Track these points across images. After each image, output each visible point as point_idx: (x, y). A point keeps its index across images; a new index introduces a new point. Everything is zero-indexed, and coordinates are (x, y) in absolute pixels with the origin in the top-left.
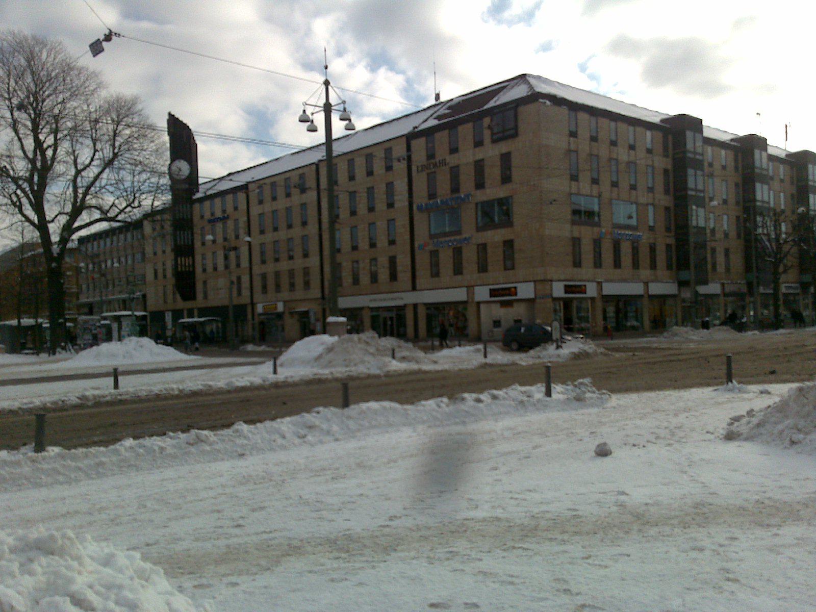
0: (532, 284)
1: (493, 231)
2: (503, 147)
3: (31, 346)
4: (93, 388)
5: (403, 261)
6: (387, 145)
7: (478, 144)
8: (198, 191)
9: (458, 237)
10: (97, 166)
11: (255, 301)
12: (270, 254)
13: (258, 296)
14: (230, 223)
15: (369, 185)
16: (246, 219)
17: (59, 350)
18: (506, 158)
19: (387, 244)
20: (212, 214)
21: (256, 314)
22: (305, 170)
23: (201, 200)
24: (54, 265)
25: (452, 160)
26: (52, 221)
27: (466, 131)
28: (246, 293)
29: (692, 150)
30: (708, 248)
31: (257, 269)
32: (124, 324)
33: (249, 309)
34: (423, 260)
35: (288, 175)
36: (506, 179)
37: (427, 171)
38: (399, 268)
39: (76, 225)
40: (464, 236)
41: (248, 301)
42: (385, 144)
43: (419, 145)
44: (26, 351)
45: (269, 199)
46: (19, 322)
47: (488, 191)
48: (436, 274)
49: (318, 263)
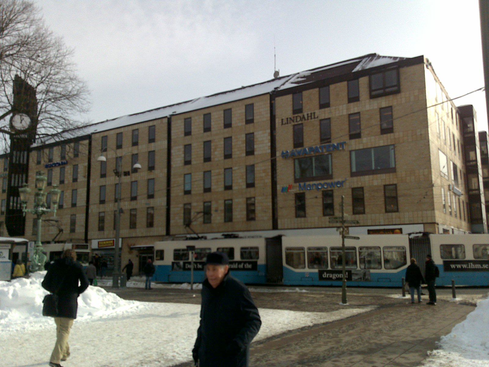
0: (422, 225)
1: (371, 176)
2: (383, 102)
5: (263, 204)
6: (188, 116)
7: (353, 98)
8: (35, 142)
9: (329, 181)
13: (93, 232)
14: (69, 169)
15: (227, 135)
16: (86, 164)
19: (244, 186)
20: (50, 160)
22: (155, 123)
23: (38, 149)
25: (323, 114)
27: (339, 90)
29: (194, 180)
31: (94, 209)
34: (287, 203)
35: (135, 127)
36: (387, 130)
37: (293, 124)
38: (258, 208)
40: (336, 180)
42: (246, 100)
43: (285, 107)
47: (364, 140)
49: (164, 203)
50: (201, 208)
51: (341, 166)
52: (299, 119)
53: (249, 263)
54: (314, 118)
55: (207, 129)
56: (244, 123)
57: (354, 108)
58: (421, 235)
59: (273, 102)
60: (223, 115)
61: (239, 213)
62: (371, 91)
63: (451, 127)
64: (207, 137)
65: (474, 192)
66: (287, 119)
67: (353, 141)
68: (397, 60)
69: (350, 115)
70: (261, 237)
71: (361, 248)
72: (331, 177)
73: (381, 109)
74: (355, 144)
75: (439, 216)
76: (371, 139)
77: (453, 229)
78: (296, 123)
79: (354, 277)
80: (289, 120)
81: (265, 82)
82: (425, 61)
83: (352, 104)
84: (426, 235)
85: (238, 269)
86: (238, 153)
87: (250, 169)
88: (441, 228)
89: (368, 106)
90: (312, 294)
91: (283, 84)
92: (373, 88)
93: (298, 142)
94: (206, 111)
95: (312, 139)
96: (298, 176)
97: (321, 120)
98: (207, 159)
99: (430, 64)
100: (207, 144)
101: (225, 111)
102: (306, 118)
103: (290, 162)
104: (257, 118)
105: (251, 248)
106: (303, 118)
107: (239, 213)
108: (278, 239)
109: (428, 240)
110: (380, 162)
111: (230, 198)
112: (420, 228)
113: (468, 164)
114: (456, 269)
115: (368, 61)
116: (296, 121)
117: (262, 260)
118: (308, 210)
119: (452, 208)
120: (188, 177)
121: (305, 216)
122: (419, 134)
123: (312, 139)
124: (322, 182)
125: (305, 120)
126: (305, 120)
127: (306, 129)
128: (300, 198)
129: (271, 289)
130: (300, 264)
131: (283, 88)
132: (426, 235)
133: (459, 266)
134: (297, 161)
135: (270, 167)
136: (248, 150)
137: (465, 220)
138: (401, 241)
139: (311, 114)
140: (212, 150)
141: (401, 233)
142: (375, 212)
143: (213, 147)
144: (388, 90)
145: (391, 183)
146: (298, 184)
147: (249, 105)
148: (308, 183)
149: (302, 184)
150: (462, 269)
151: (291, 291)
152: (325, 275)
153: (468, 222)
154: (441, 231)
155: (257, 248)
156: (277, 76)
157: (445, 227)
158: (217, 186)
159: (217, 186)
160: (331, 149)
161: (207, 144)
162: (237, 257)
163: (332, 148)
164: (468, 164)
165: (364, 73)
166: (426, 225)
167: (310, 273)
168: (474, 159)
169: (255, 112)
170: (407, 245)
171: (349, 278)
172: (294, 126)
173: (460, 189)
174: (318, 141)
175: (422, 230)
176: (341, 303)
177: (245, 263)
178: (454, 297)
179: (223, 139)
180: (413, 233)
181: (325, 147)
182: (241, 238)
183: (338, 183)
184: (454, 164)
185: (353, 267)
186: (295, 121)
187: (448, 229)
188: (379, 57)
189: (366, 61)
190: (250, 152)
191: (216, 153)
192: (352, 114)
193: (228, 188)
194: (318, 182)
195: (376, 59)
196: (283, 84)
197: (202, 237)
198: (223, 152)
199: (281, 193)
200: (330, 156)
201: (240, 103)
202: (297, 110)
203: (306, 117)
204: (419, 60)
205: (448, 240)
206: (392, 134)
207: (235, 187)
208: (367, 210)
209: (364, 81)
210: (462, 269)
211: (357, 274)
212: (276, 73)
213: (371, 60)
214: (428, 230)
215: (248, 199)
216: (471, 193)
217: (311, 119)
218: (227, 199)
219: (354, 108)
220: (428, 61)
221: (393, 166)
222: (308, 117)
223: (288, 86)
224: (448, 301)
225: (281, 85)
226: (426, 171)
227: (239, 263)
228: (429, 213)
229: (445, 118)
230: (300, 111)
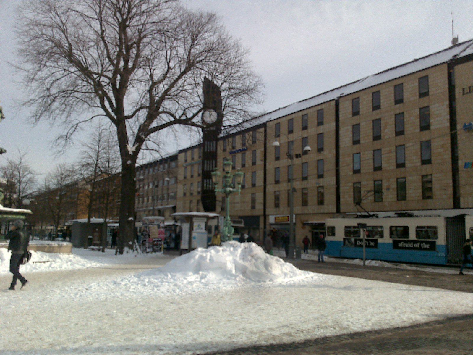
3: (98, 242)
6: (356, 96)
8: (221, 133)
10: (178, 69)
11: (267, 213)
12: (283, 176)
14: (248, 154)
16: (263, 149)
17: (126, 249)
20: (234, 147)
21: (267, 223)
22: (323, 106)
23: (224, 138)
24: (129, 162)
26: (131, 117)
28: (259, 206)
30: (109, 230)
31: (270, 189)
32: (196, 225)
33: (262, 220)
35: (304, 112)
38: (436, 186)
39: (154, 124)
41: (261, 213)
44: (92, 247)
45: (286, 132)
46: (89, 220)
49: (334, 182)
50: (371, 186)
53: (427, 243)
55: (376, 107)
56: (418, 97)
59: (451, 71)
61: (414, 191)
70: (439, 216)
85: (414, 248)
87: (426, 145)
91: (464, 50)
94: (375, 89)
100: (377, 123)
107: (414, 191)
117: (441, 240)
131: (463, 54)
140: (382, 128)
147: (423, 79)
155: (435, 228)
156: (455, 43)
158: (388, 163)
159: (388, 163)
161: (377, 123)
162: (412, 236)
177: (422, 242)
179: (394, 116)
182: (417, 216)
190: (425, 126)
191: (386, 131)
196: (464, 50)
197: (374, 215)
201: (412, 77)
207: (408, 165)
212: (455, 40)
218: (398, 177)
227: (415, 242)
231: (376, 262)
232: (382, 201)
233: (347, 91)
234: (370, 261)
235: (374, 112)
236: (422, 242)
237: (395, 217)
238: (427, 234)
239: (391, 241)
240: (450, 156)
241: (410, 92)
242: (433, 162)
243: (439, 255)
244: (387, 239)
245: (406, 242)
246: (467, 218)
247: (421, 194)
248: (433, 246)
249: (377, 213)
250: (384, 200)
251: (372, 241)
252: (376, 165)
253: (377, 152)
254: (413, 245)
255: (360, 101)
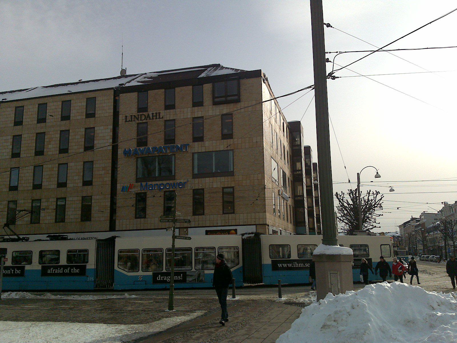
1: (211, 179)
2: (225, 109)
4: (435, 293)
5: (100, 205)
6: (20, 104)
7: (198, 103)
9: (171, 182)
18: (227, 117)
19: (81, 184)
25: (169, 115)
27: (184, 93)
34: (126, 203)
36: (227, 136)
37: (138, 122)
38: (95, 208)
40: (178, 181)
43: (129, 104)
47: (207, 143)
48: (141, 212)
50: (28, 206)
51: (183, 168)
52: (143, 118)
53: (77, 267)
54: (159, 118)
55: (42, 120)
56: (84, 117)
57: (198, 112)
58: (253, 235)
59: (117, 98)
60: (60, 107)
61: (73, 212)
62: (214, 97)
63: (282, 139)
64: (41, 128)
65: (299, 198)
66: (131, 116)
67: (196, 144)
68: (239, 71)
69: (194, 118)
70: (92, 238)
71: (197, 249)
72: (174, 178)
73: (223, 115)
74: (197, 147)
75: (270, 219)
76: (212, 144)
77: (281, 231)
78: (140, 122)
79: (189, 279)
80: (133, 117)
81: (111, 79)
82: (262, 75)
83: (196, 108)
84: (257, 235)
85: (64, 274)
86: (76, 147)
87: (88, 165)
88: (271, 229)
89: (211, 112)
90: (141, 299)
91: (129, 82)
92: (216, 96)
93: (142, 142)
94: (42, 101)
95: (156, 140)
96: (140, 176)
97: (166, 121)
98: (39, 152)
99: (267, 79)
100: (40, 137)
101: (63, 102)
102: (151, 118)
103: (133, 160)
104: (98, 113)
105: (80, 251)
106: (147, 117)
107: (73, 212)
108: (112, 241)
109: (259, 240)
110: (218, 165)
111: (63, 196)
112: (252, 229)
113: (295, 173)
114: (283, 269)
115: (212, 70)
116: (141, 120)
117: (91, 264)
118: (149, 211)
119: (281, 212)
120: (15, 172)
121: (145, 217)
122: (255, 141)
123: (156, 140)
124: (165, 182)
125: (150, 119)
126: (150, 119)
127: (151, 129)
128: (141, 199)
129: (96, 295)
130: (134, 267)
131: (128, 85)
132: (257, 235)
133: (285, 265)
134: (139, 160)
135: (110, 164)
136: (86, 145)
137: (291, 222)
138: (234, 241)
139: (156, 113)
140: (46, 143)
141: (236, 234)
142: (213, 214)
143: (46, 140)
144: (229, 98)
145: (229, 186)
146: (139, 183)
147: (91, 99)
148: (150, 183)
149: (144, 184)
150: (288, 269)
151: (119, 297)
152: (159, 278)
153: (294, 225)
154: (271, 232)
155: (86, 251)
156: (123, 74)
157: (275, 229)
158: (49, 182)
159: (49, 182)
160: (175, 150)
161: (40, 137)
162: (63, 261)
163: (175, 149)
164: (295, 173)
165: (209, 80)
166: (258, 226)
167: (144, 276)
168: (300, 169)
169: (97, 106)
170: (240, 245)
171: (184, 281)
172: (138, 124)
173: (288, 194)
174: (162, 141)
175: (254, 231)
176: (167, 310)
177: (72, 267)
178: (280, 296)
179: (59, 132)
180: (246, 234)
181: (169, 147)
182: (70, 239)
183: (180, 184)
184: (283, 172)
185: (189, 268)
186: (140, 119)
187: (277, 230)
188: (223, 68)
189: (211, 70)
190: (89, 147)
191: (50, 146)
192: (196, 118)
193: (62, 185)
194: (161, 182)
195: (219, 70)
196: (129, 82)
197: (24, 239)
198: (58, 146)
199: (121, 193)
200: (173, 157)
201: (81, 96)
202: (142, 109)
203: (151, 116)
204: (257, 74)
205: (277, 240)
206: (232, 140)
207: (70, 185)
208: (206, 211)
209: (207, 87)
210: (288, 269)
211: (191, 276)
212: (123, 71)
213: (215, 70)
214: (260, 231)
215: (83, 198)
216: (296, 198)
217: (156, 118)
218: (59, 197)
219: (198, 112)
220: (264, 76)
221: (232, 170)
222: (153, 116)
223: (134, 83)
224: (274, 301)
225: (127, 83)
226: (260, 175)
227: (65, 267)
228: (261, 214)
229: (278, 130)
230: (145, 109)
231: (16, 294)
232: (39, 223)
233: (10, 97)
234: (9, 293)
235: (39, 125)
236: (72, 267)
237: (48, 240)
238: (77, 258)
239: (39, 267)
240: (110, 179)
241: (78, 109)
242: (94, 184)
243: (89, 279)
244: (35, 266)
245: (56, 268)
246: (117, 240)
247: (80, 216)
248: (83, 271)
249: (27, 236)
250: (41, 222)
251: (18, 268)
252: (36, 183)
253: (38, 168)
254: (63, 271)
255: (24, 111)
